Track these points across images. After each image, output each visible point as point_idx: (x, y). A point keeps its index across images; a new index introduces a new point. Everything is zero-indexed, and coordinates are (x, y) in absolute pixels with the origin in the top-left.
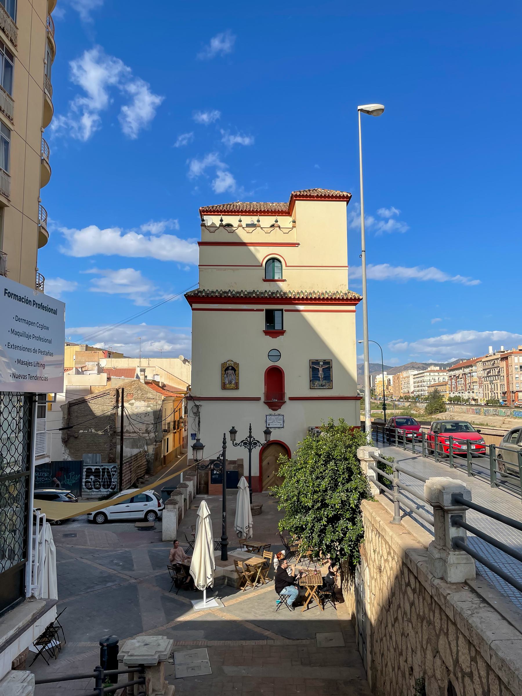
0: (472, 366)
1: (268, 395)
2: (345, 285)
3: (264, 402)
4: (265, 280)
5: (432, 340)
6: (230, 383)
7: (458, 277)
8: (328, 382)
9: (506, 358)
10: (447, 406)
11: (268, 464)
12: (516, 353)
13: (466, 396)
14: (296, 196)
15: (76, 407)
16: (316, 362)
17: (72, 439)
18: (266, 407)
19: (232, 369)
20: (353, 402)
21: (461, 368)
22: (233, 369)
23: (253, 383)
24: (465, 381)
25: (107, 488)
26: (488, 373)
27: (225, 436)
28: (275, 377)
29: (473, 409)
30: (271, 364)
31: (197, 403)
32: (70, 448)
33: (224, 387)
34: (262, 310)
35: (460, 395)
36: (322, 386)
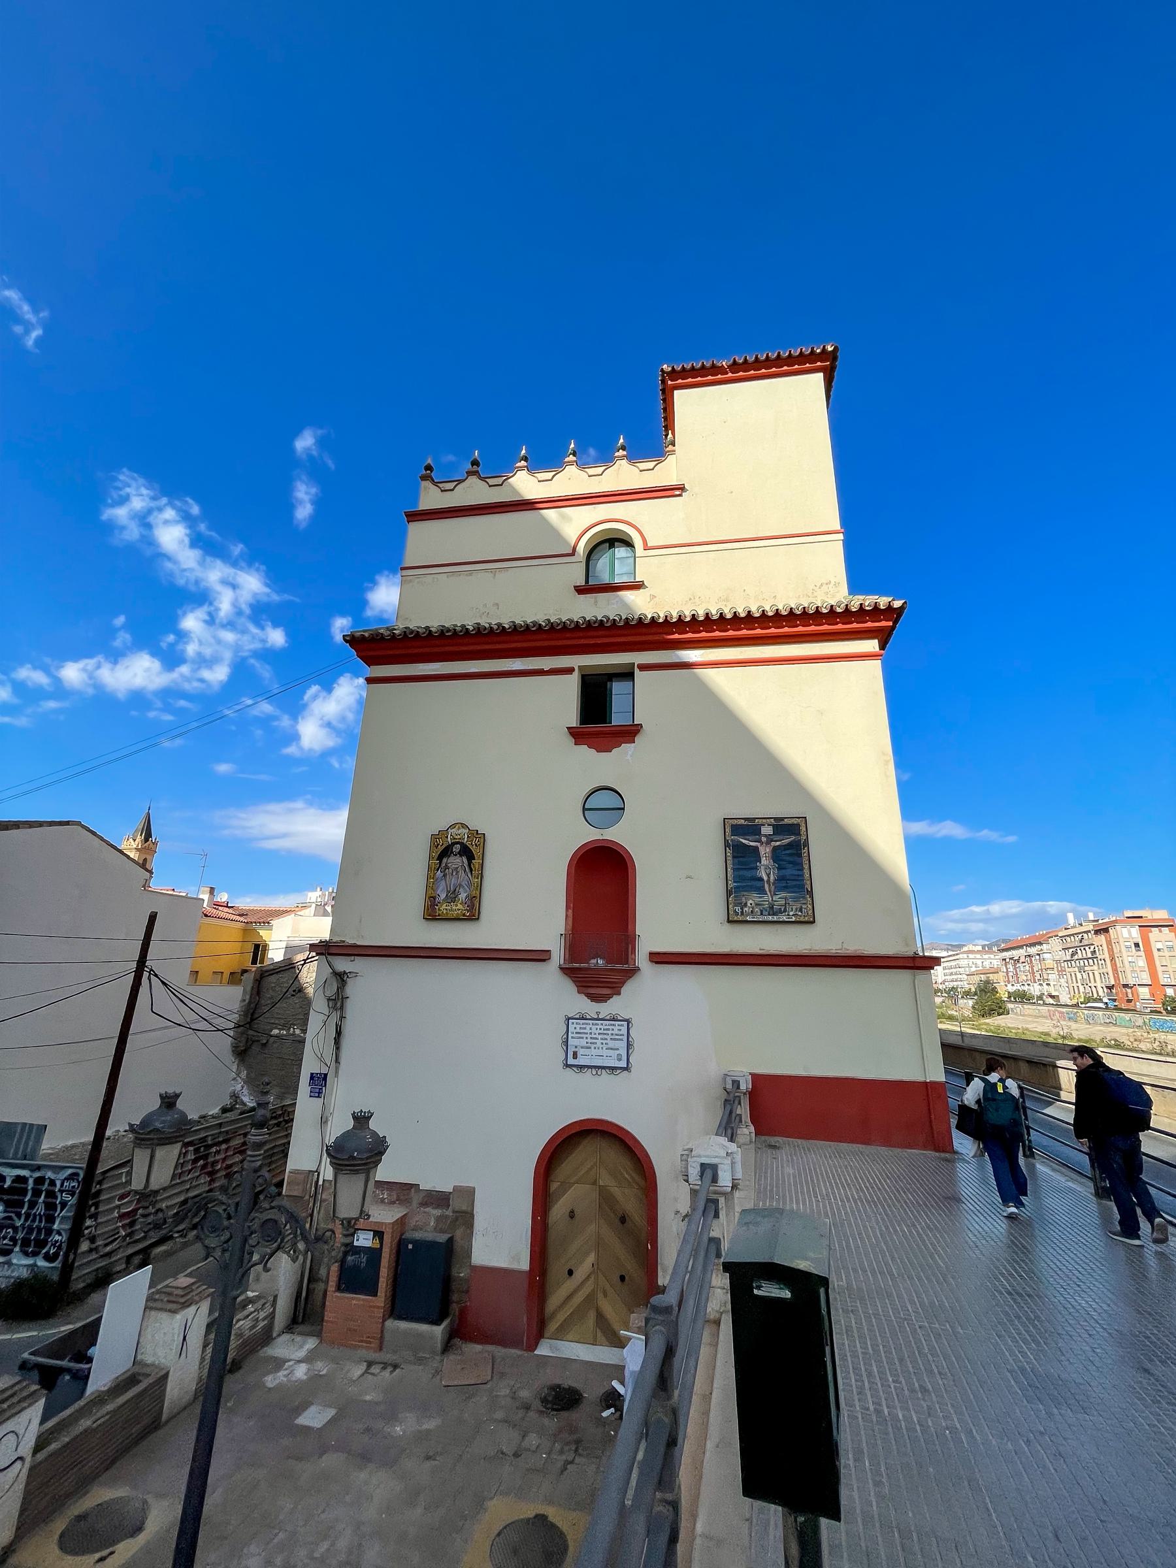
0: (1040, 944)
1: (576, 945)
2: (837, 584)
3: (561, 968)
4: (580, 590)
5: (956, 913)
6: (452, 897)
7: (985, 833)
8: (796, 899)
9: (1106, 930)
10: (1010, 1006)
11: (572, 1215)
12: (1122, 921)
13: (1035, 990)
14: (674, 374)
15: (273, 979)
16: (749, 827)
17: (255, 1048)
18: (568, 987)
19: (461, 854)
20: (904, 976)
21: (1021, 947)
22: (466, 852)
23: (528, 901)
24: (1032, 967)
25: (35, 1254)
26: (1073, 955)
28: (602, 877)
29: (1061, 1013)
30: (590, 835)
31: (342, 964)
32: (249, 1068)
33: (432, 914)
34: (569, 671)
35: (1026, 988)
36: (772, 911)
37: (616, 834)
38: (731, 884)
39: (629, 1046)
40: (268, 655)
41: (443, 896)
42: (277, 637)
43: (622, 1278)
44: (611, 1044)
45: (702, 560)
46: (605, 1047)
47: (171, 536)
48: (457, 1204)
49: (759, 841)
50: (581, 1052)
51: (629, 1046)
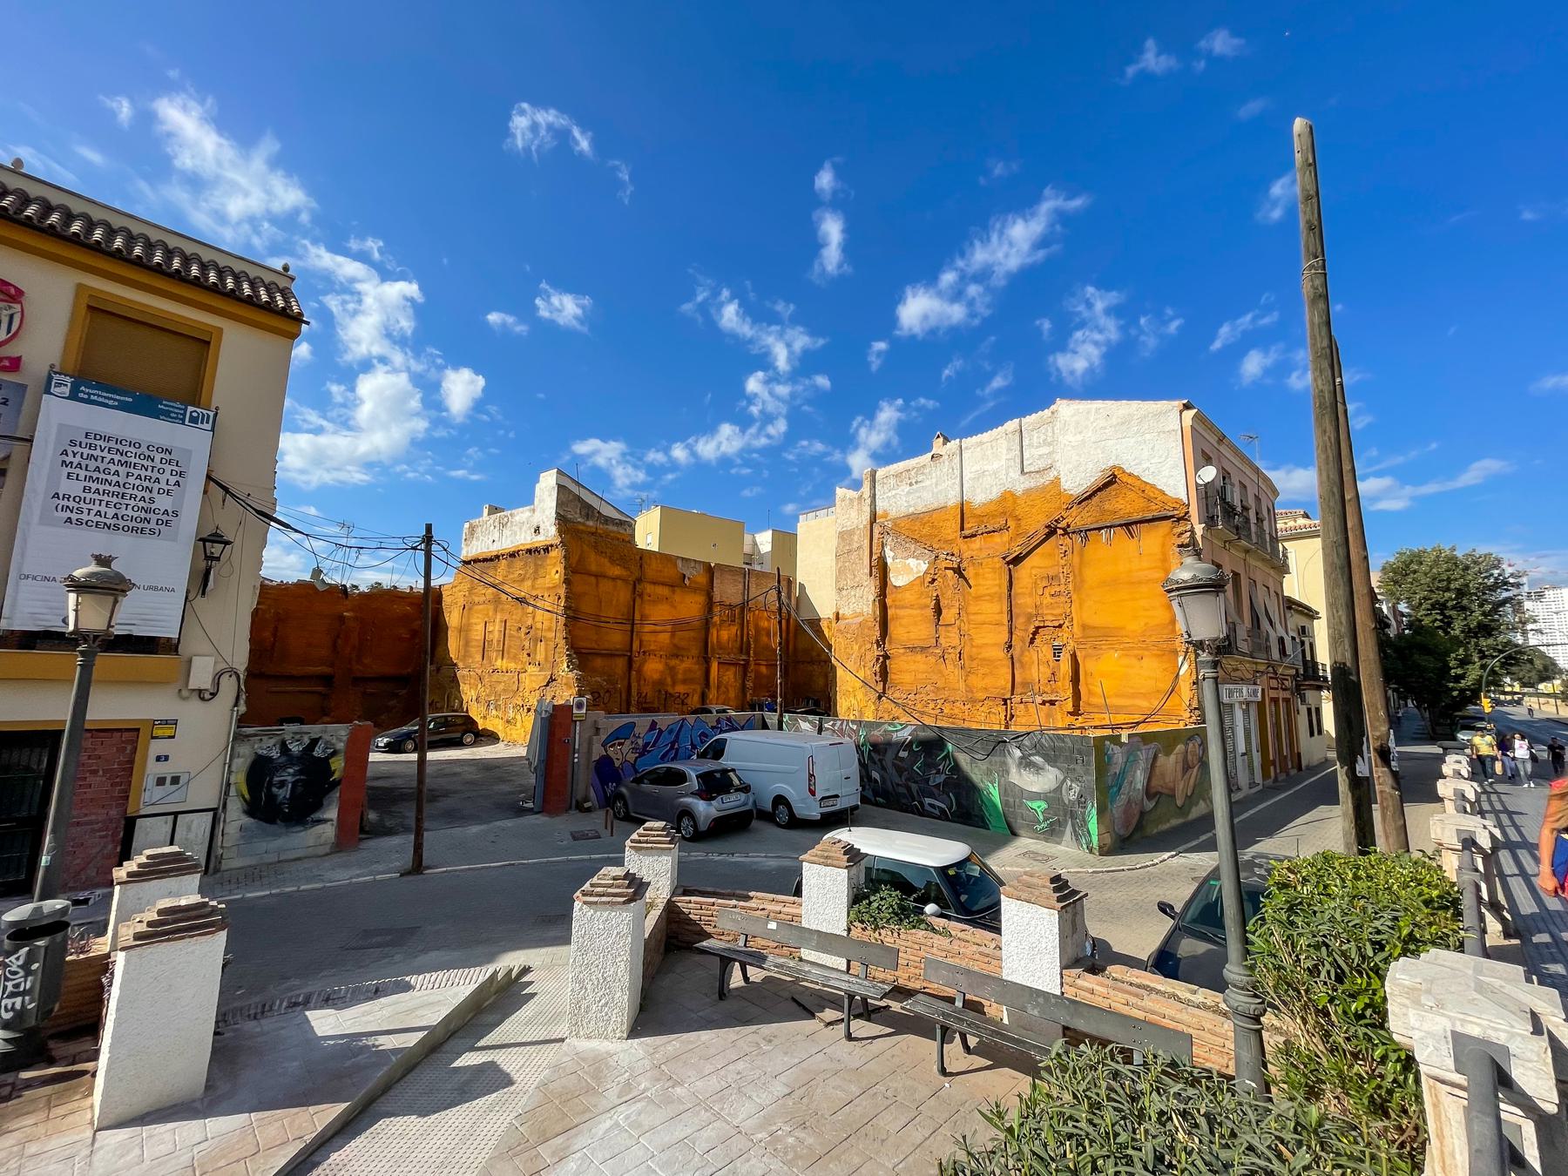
40: (819, 398)
42: (823, 381)
47: (730, 315)
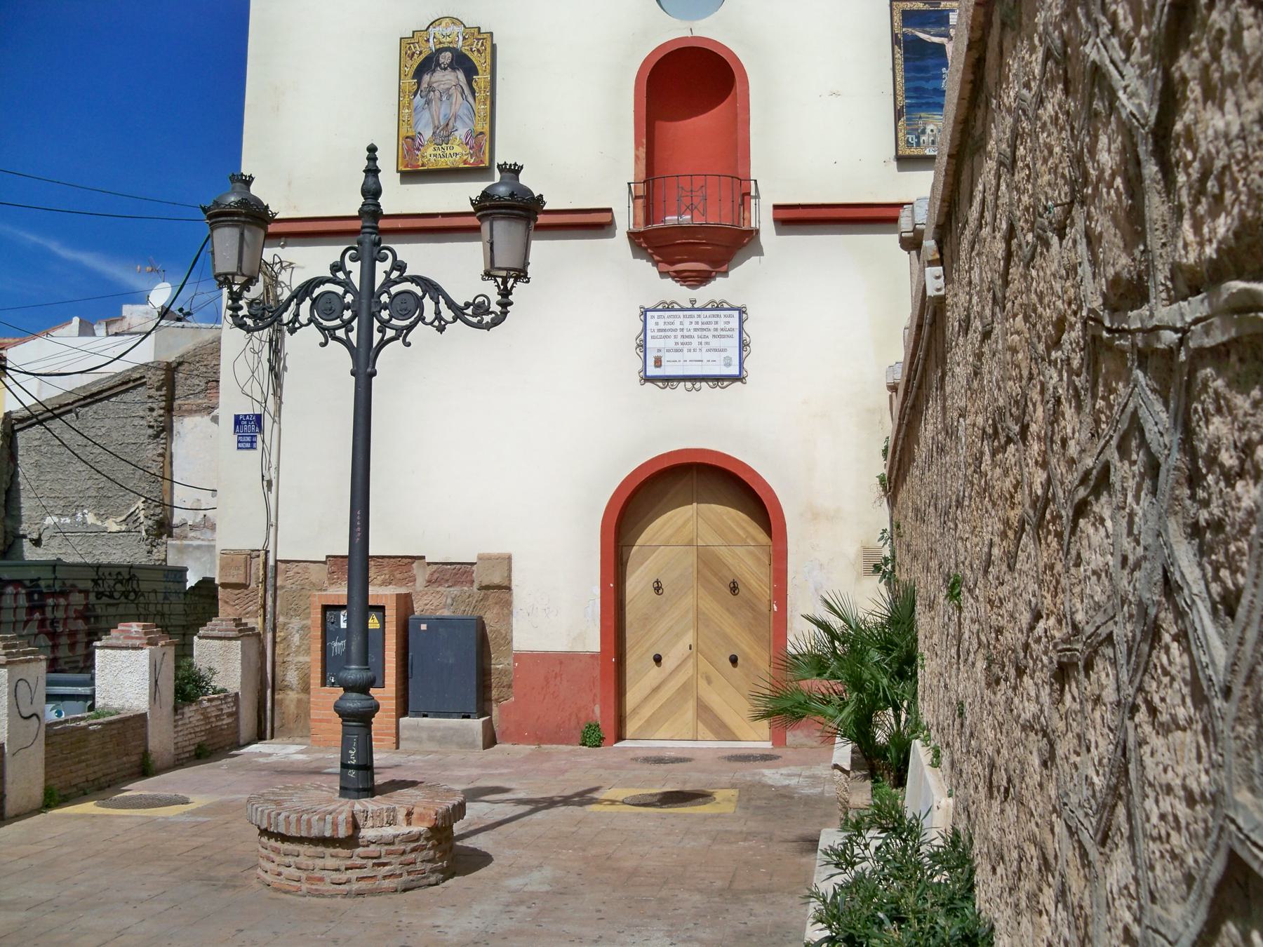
6: (444, 135)
18: (646, 269)
19: (453, 66)
22: (462, 63)
27: (372, 158)
30: (672, 30)
37: (709, 29)
38: (902, 101)
39: (743, 345)
41: (427, 134)
43: (734, 660)
44: (715, 343)
45: (824, 210)
46: (705, 348)
48: (483, 576)
49: (947, 35)
50: (666, 357)
51: (743, 345)
